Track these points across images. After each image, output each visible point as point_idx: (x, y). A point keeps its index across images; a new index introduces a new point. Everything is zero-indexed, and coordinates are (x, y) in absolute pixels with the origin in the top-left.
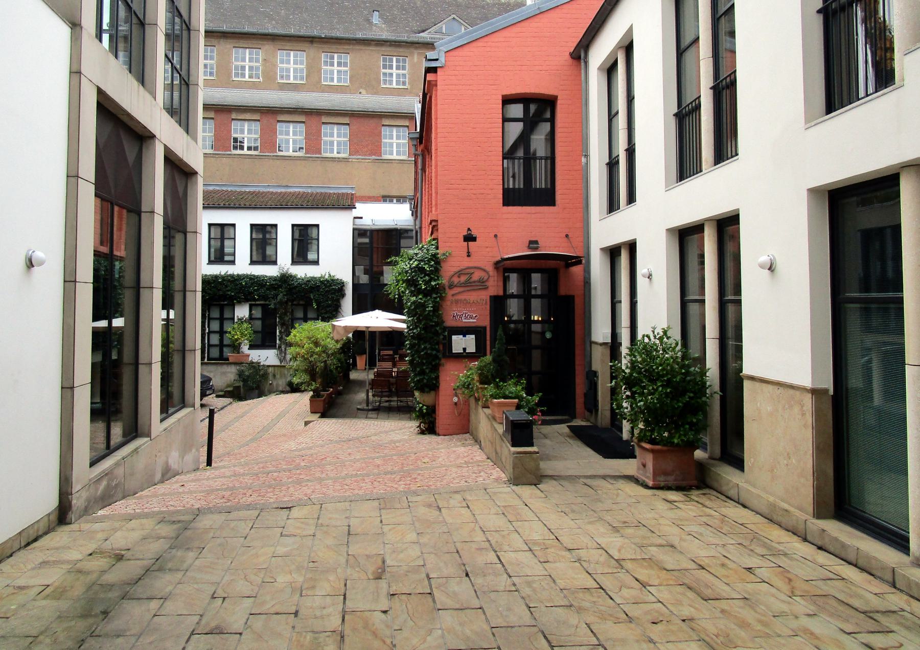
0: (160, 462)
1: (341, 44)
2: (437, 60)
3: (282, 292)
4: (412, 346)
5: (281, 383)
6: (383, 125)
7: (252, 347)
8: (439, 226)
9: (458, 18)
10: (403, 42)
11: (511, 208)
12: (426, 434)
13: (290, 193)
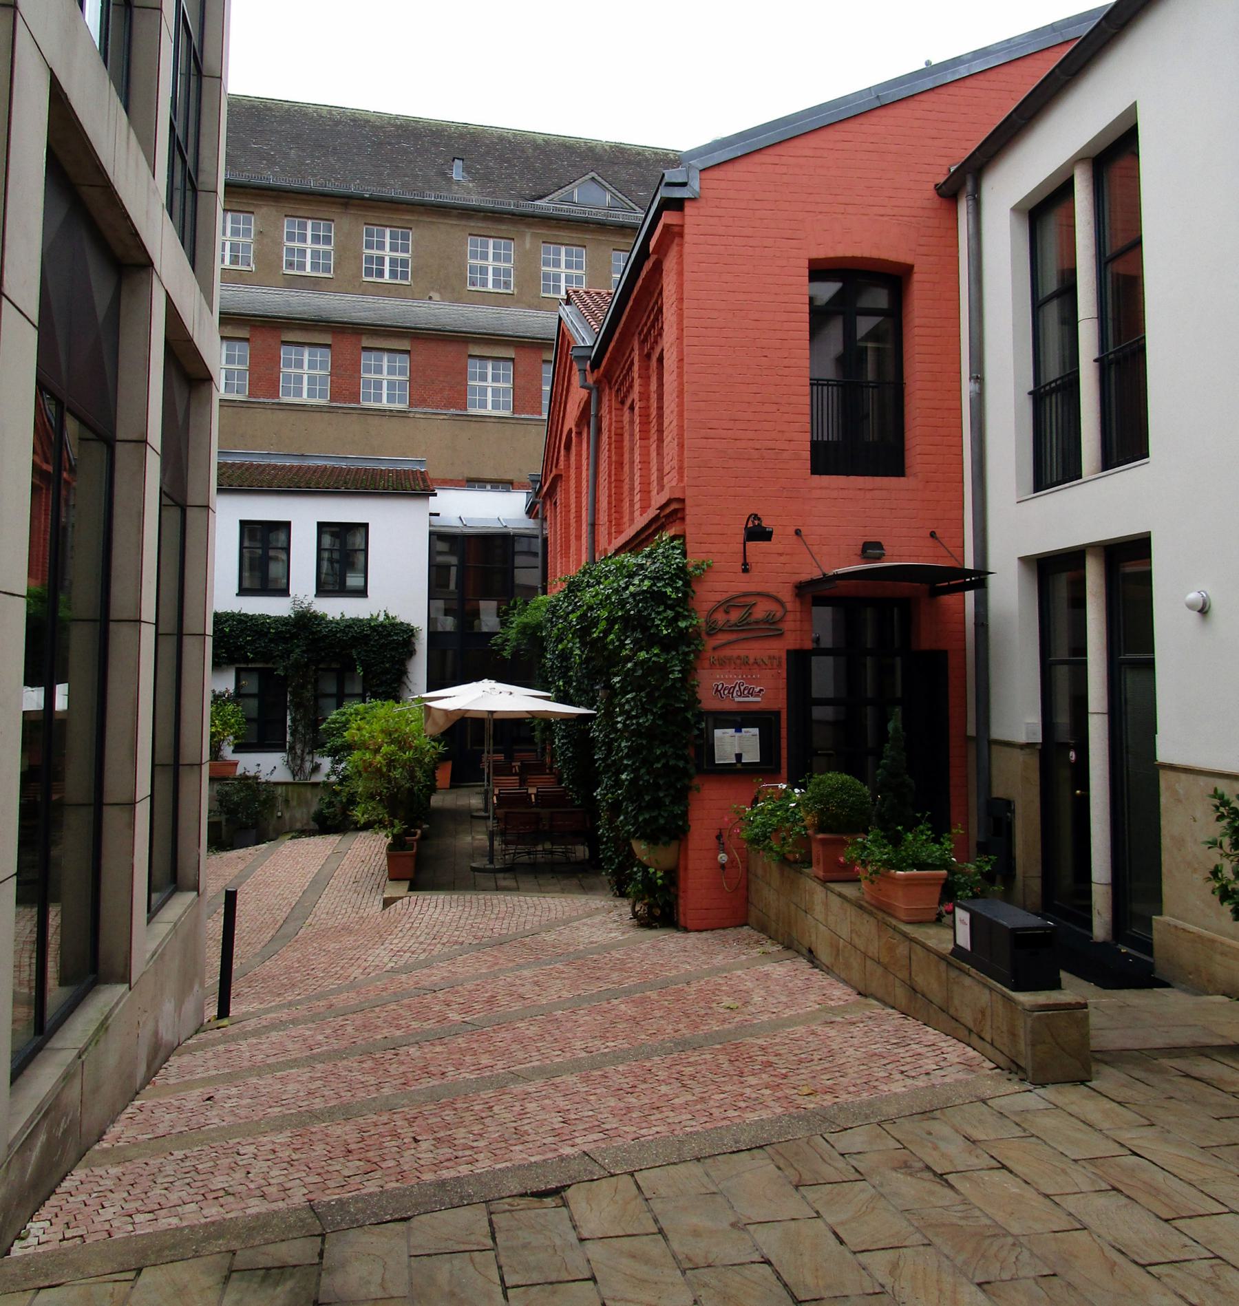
0: (146, 1033)
1: (397, 210)
2: (684, 185)
3: (298, 646)
4: (633, 752)
5: (301, 815)
6: (470, 356)
7: (238, 749)
8: (687, 512)
9: (599, 179)
10: (508, 213)
11: (825, 480)
12: (655, 928)
13: (309, 467)
